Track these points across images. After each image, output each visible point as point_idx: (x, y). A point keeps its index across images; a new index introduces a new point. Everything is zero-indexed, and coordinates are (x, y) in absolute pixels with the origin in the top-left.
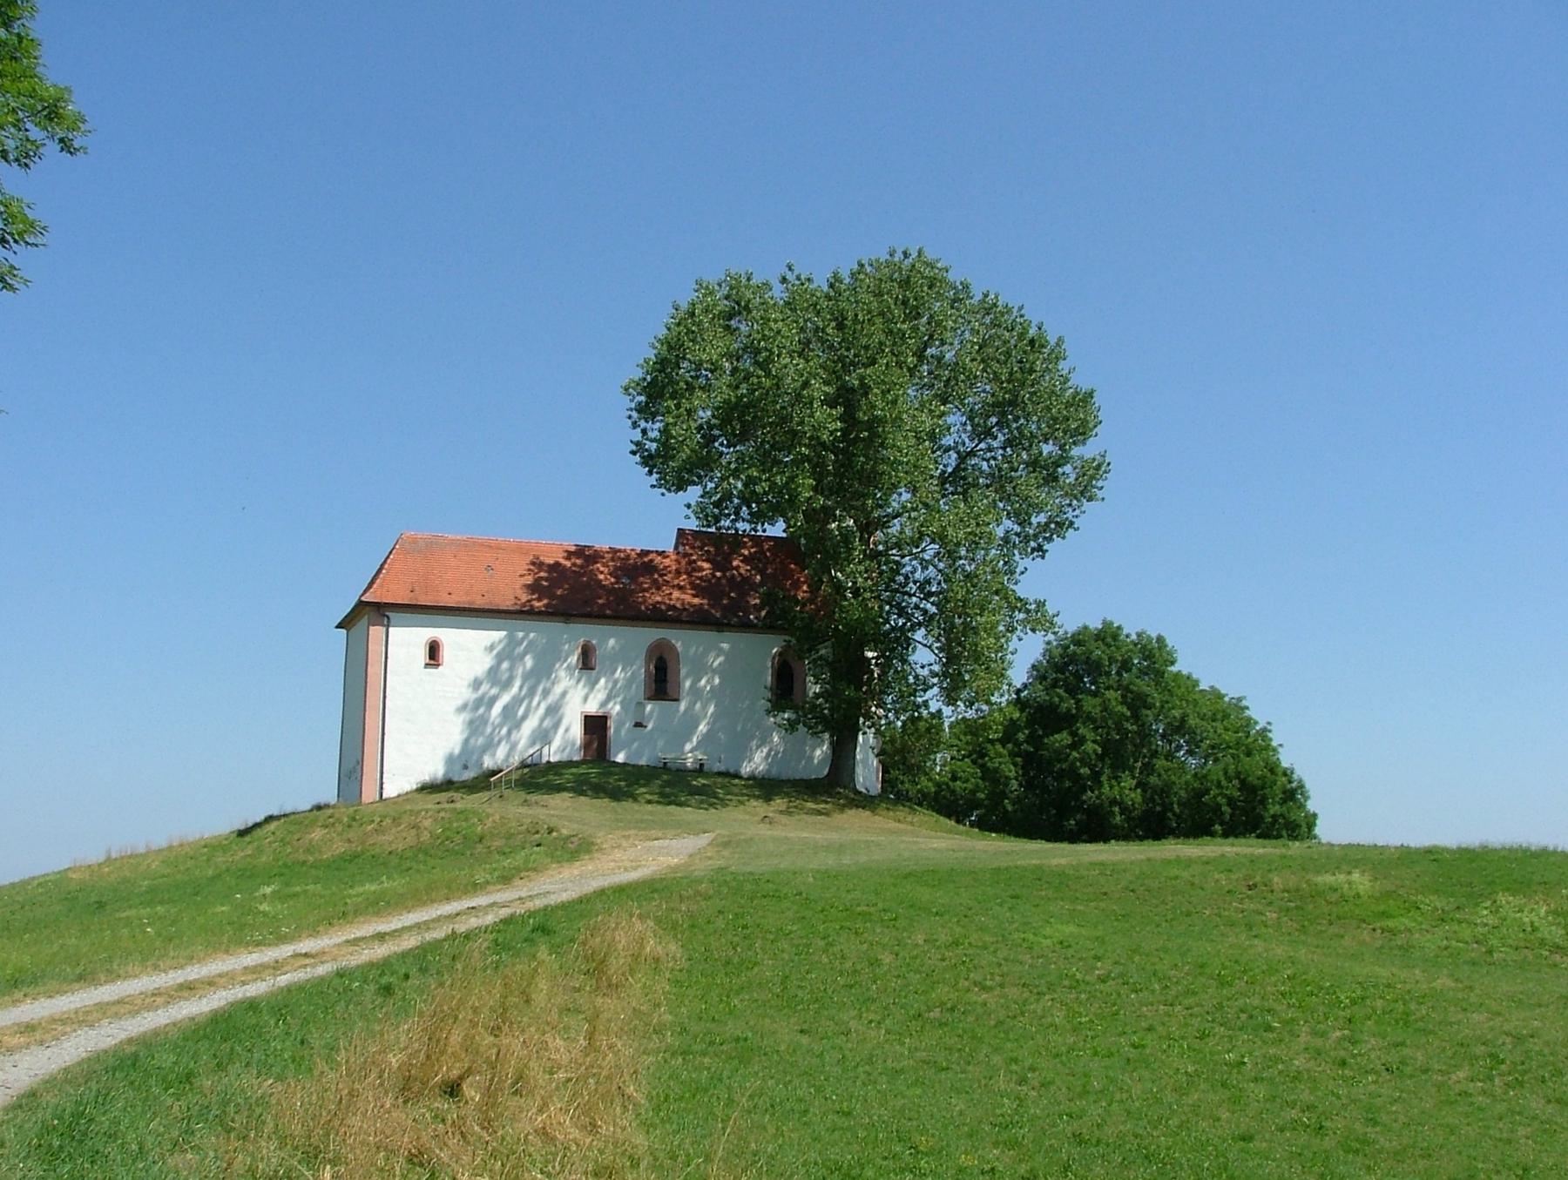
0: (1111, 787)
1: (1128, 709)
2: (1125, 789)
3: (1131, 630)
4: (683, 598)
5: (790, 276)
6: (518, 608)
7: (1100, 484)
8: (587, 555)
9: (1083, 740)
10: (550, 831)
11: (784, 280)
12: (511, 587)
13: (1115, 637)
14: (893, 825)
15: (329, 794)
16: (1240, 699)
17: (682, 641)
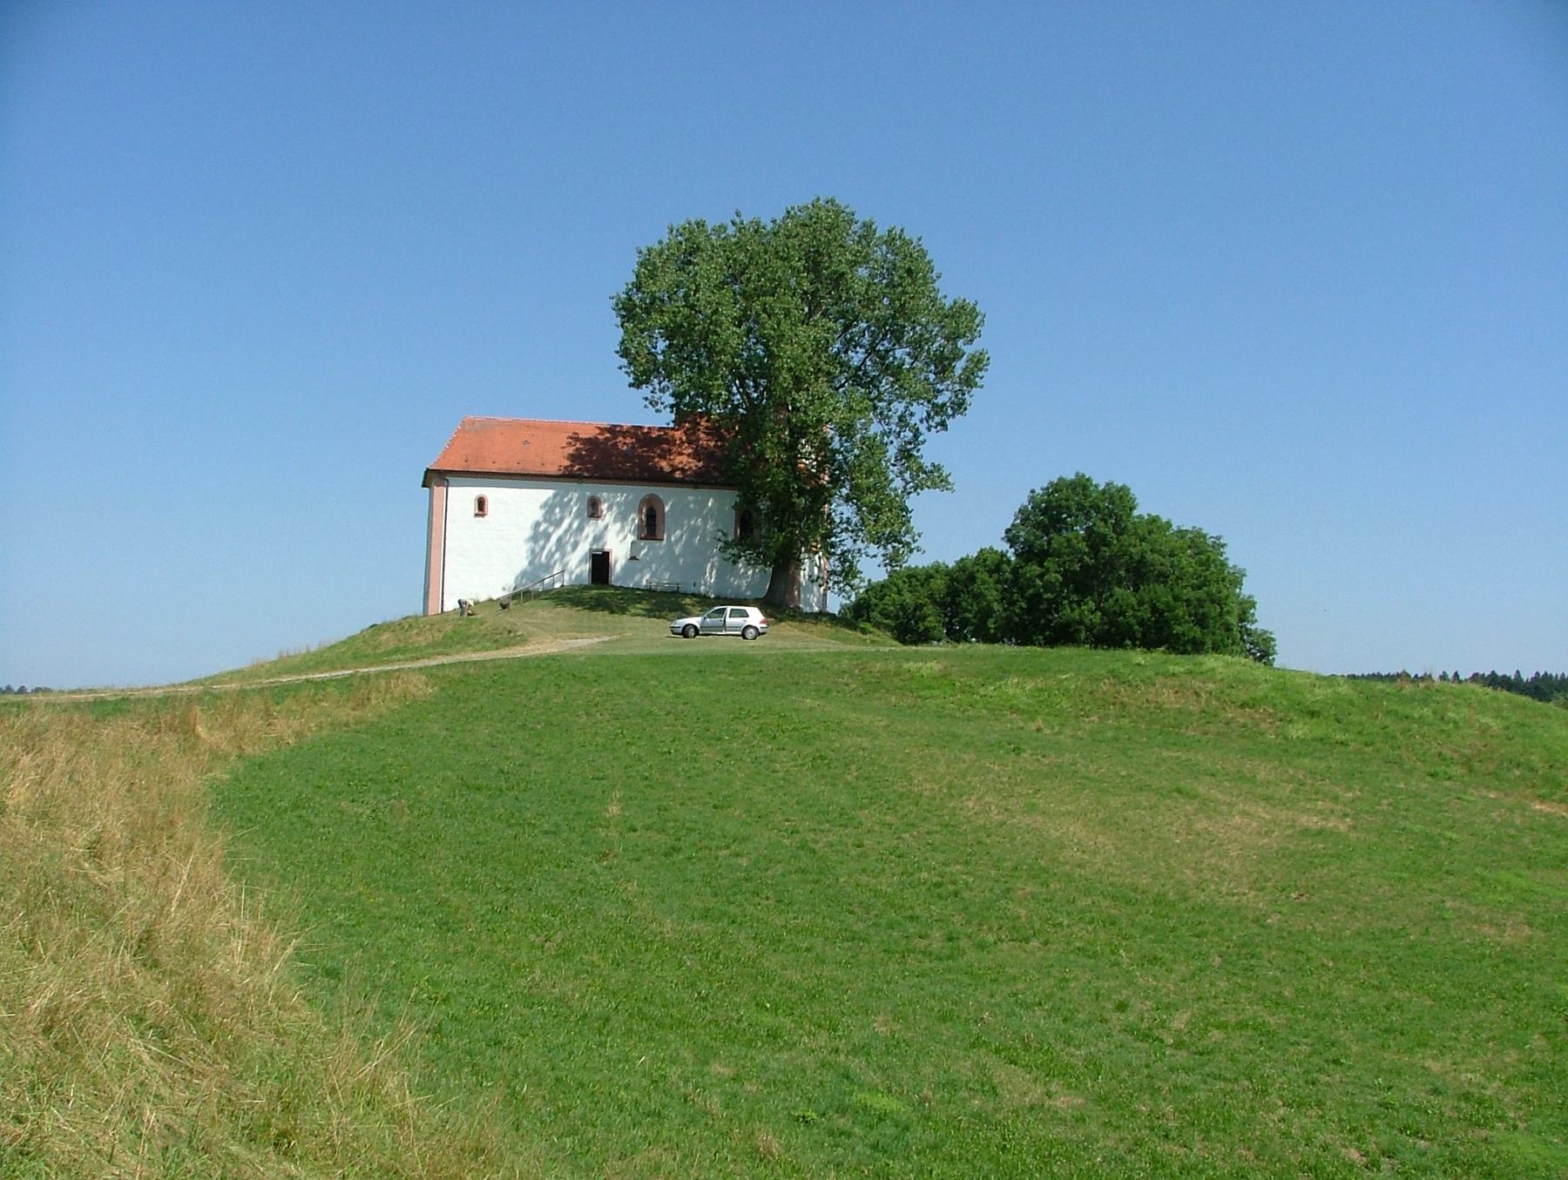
0: (1072, 610)
1: (1087, 545)
2: (1087, 612)
3: (1100, 480)
4: (684, 460)
5: (737, 220)
6: (560, 473)
7: (980, 374)
8: (613, 430)
9: (1048, 570)
10: (510, 632)
11: (734, 223)
12: (557, 460)
13: (1085, 488)
14: (797, 632)
15: (420, 611)
16: (1218, 538)
17: (670, 500)
